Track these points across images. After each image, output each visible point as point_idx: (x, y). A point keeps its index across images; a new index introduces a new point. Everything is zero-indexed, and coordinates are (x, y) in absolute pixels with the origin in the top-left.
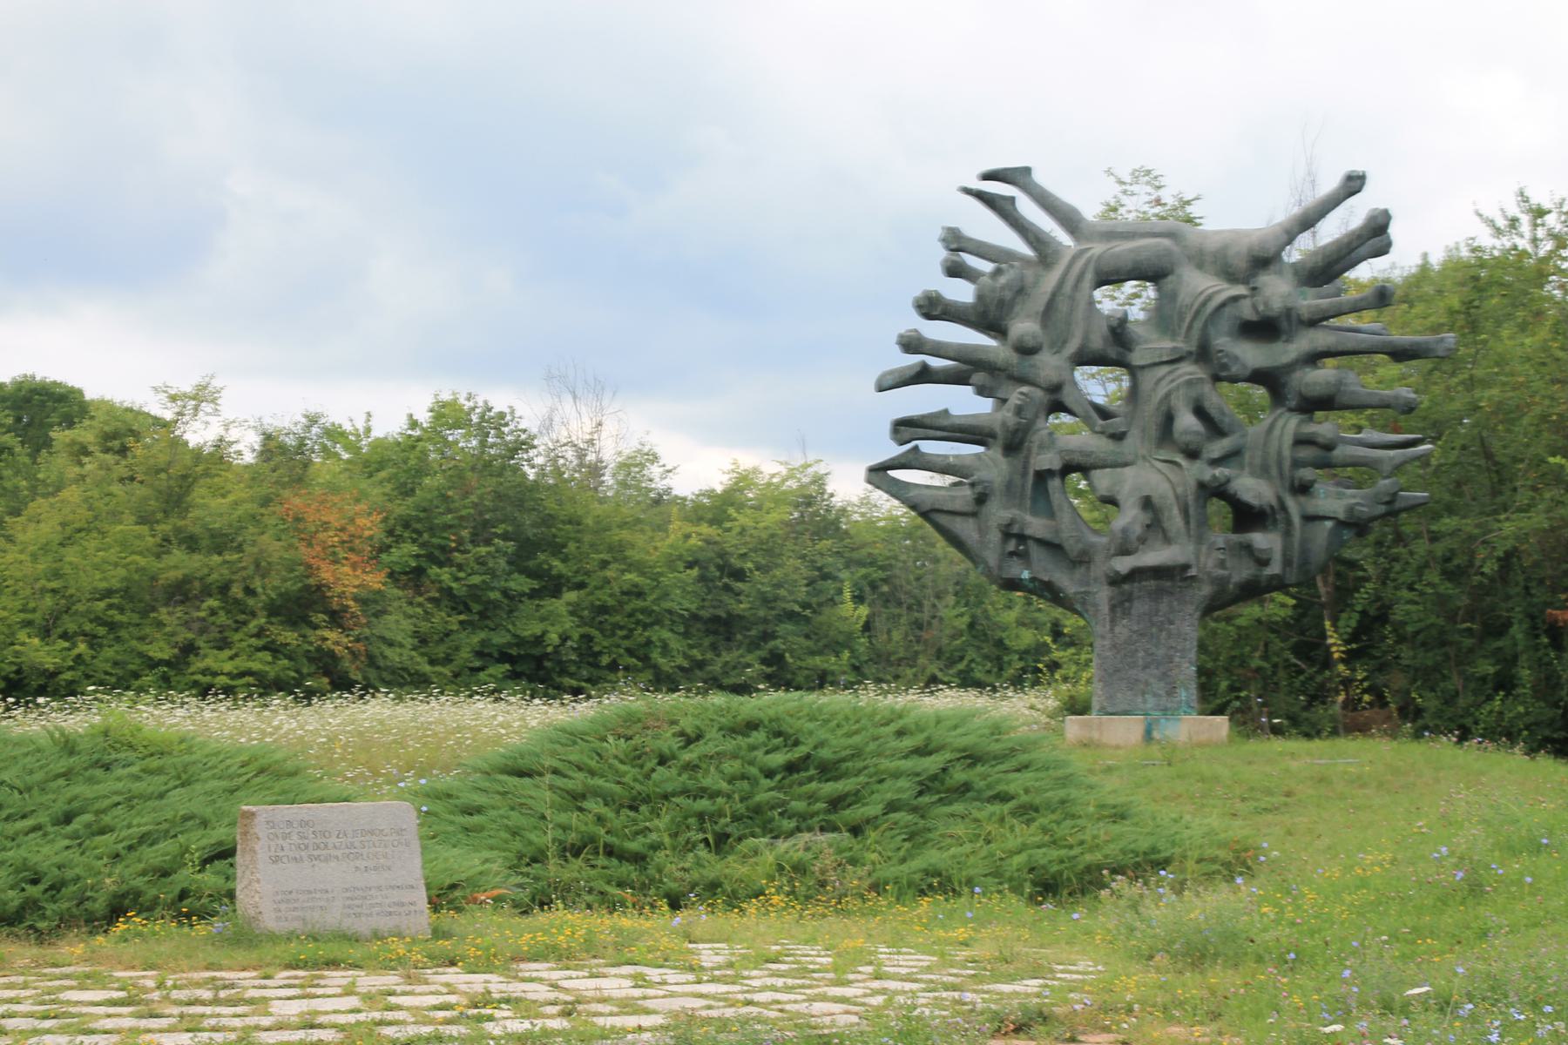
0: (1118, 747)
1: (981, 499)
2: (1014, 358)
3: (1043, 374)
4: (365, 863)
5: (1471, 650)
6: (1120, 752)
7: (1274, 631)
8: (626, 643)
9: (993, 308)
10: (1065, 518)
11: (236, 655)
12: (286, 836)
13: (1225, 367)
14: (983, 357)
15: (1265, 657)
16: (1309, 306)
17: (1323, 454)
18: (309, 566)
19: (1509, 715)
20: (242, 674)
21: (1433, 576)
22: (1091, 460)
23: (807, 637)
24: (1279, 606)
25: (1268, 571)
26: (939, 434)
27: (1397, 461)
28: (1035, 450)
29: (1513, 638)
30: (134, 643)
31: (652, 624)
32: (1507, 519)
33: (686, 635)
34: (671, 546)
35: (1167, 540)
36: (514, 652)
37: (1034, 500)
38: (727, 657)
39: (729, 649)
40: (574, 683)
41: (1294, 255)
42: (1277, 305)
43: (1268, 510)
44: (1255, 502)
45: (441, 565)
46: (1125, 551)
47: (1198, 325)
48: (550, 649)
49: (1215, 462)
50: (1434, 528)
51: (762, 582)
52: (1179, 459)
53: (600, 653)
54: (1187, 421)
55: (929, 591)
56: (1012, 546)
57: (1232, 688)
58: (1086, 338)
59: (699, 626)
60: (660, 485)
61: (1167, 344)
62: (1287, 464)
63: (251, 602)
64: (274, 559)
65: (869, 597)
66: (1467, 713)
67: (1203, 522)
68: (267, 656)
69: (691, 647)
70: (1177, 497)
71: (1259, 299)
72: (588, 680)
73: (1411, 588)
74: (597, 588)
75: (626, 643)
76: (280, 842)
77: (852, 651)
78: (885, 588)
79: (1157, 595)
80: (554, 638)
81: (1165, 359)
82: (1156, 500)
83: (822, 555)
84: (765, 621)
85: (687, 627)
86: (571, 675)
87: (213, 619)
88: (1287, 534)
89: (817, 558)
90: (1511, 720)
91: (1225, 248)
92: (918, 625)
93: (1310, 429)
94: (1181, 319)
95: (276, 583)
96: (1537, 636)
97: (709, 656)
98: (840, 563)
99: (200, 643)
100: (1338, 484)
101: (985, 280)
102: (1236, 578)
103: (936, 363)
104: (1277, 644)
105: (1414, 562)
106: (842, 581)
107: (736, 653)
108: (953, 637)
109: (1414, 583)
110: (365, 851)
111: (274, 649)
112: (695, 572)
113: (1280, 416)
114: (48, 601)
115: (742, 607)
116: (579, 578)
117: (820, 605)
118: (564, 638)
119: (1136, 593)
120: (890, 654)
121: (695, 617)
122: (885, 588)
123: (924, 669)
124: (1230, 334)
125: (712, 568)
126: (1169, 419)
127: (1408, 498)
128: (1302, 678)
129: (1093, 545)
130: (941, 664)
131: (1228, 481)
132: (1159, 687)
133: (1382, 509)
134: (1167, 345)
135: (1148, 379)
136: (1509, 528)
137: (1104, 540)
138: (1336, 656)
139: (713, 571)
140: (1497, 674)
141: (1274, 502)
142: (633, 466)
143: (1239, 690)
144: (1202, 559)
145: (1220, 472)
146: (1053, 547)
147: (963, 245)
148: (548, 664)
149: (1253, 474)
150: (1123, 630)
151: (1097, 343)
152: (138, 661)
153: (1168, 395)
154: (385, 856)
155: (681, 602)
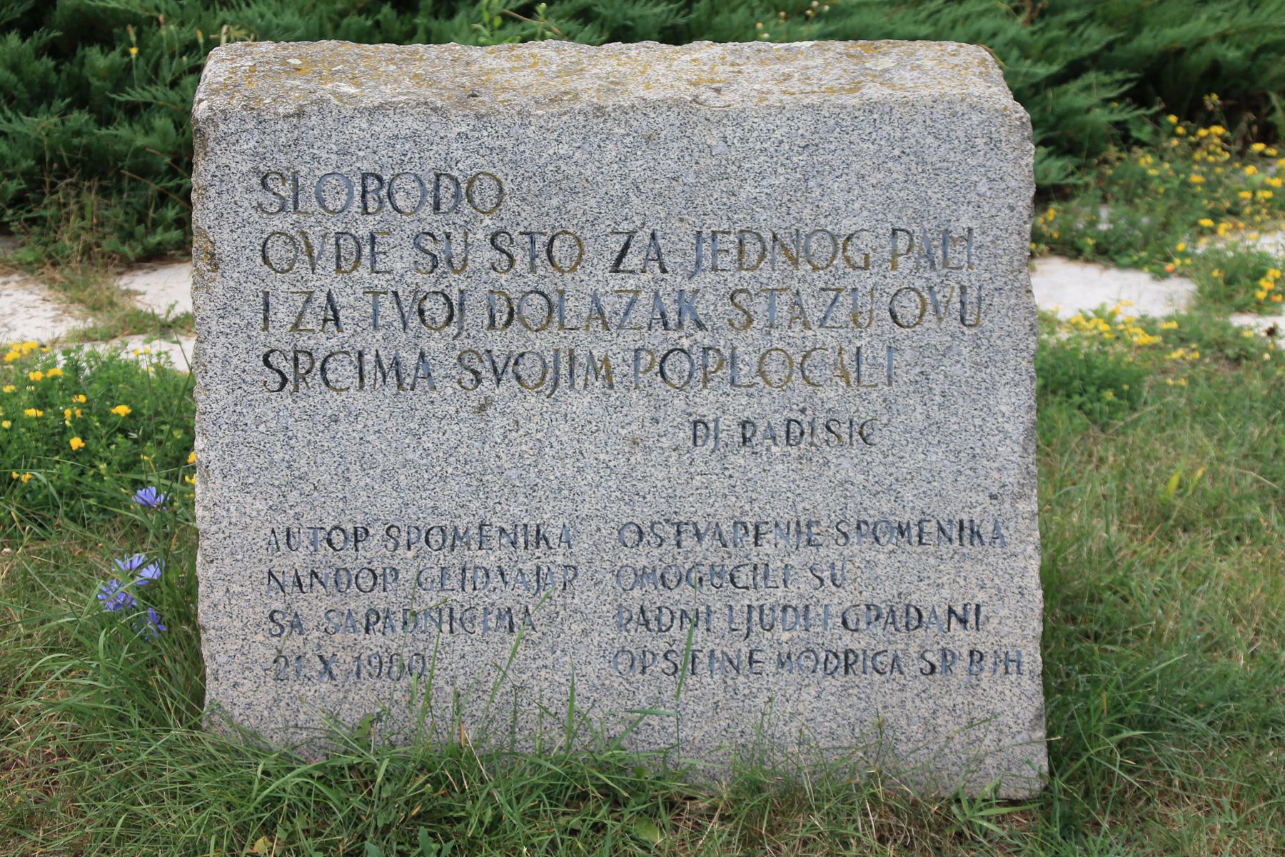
4: (740, 405)
12: (358, 252)
76: (325, 279)
110: (747, 345)
154: (851, 371)
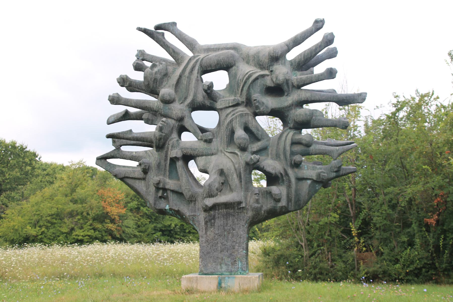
1: (145, 171)
2: (161, 105)
3: (174, 112)
5: (399, 232)
9: (151, 83)
11: (85, 231)
13: (257, 107)
17: (306, 147)
18: (104, 207)
19: (412, 255)
20: (86, 236)
21: (385, 207)
22: (196, 153)
25: (280, 205)
27: (340, 152)
28: (170, 148)
29: (413, 228)
30: (58, 228)
32: (410, 187)
35: (231, 190)
36: (164, 229)
37: (170, 172)
40: (179, 237)
42: (281, 78)
43: (279, 175)
44: (273, 172)
45: (144, 207)
46: (211, 195)
47: (246, 88)
48: (172, 228)
52: (237, 151)
53: (186, 229)
54: (240, 133)
57: (318, 246)
58: (195, 95)
61: (233, 98)
62: (288, 154)
63: (88, 217)
64: (94, 205)
66: (398, 254)
68: (92, 231)
70: (236, 170)
71: (274, 76)
73: (378, 211)
79: (227, 216)
80: (173, 225)
81: (231, 105)
82: (225, 171)
86: (179, 235)
87: (79, 221)
88: (289, 187)
90: (413, 257)
91: (258, 53)
93: (297, 137)
94: (238, 86)
95: (95, 212)
96: (422, 228)
99: (75, 228)
101: (148, 70)
102: (265, 208)
103: (132, 110)
105: (380, 202)
111: (95, 229)
114: (36, 217)
118: (176, 225)
119: (217, 216)
124: (261, 92)
126: (233, 132)
127: (346, 169)
131: (258, 161)
132: (228, 261)
133: (334, 174)
136: (410, 190)
138: (354, 234)
140: (408, 241)
143: (320, 246)
144: (248, 199)
146: (179, 194)
148: (172, 232)
151: (201, 97)
152: (59, 232)
153: (231, 121)
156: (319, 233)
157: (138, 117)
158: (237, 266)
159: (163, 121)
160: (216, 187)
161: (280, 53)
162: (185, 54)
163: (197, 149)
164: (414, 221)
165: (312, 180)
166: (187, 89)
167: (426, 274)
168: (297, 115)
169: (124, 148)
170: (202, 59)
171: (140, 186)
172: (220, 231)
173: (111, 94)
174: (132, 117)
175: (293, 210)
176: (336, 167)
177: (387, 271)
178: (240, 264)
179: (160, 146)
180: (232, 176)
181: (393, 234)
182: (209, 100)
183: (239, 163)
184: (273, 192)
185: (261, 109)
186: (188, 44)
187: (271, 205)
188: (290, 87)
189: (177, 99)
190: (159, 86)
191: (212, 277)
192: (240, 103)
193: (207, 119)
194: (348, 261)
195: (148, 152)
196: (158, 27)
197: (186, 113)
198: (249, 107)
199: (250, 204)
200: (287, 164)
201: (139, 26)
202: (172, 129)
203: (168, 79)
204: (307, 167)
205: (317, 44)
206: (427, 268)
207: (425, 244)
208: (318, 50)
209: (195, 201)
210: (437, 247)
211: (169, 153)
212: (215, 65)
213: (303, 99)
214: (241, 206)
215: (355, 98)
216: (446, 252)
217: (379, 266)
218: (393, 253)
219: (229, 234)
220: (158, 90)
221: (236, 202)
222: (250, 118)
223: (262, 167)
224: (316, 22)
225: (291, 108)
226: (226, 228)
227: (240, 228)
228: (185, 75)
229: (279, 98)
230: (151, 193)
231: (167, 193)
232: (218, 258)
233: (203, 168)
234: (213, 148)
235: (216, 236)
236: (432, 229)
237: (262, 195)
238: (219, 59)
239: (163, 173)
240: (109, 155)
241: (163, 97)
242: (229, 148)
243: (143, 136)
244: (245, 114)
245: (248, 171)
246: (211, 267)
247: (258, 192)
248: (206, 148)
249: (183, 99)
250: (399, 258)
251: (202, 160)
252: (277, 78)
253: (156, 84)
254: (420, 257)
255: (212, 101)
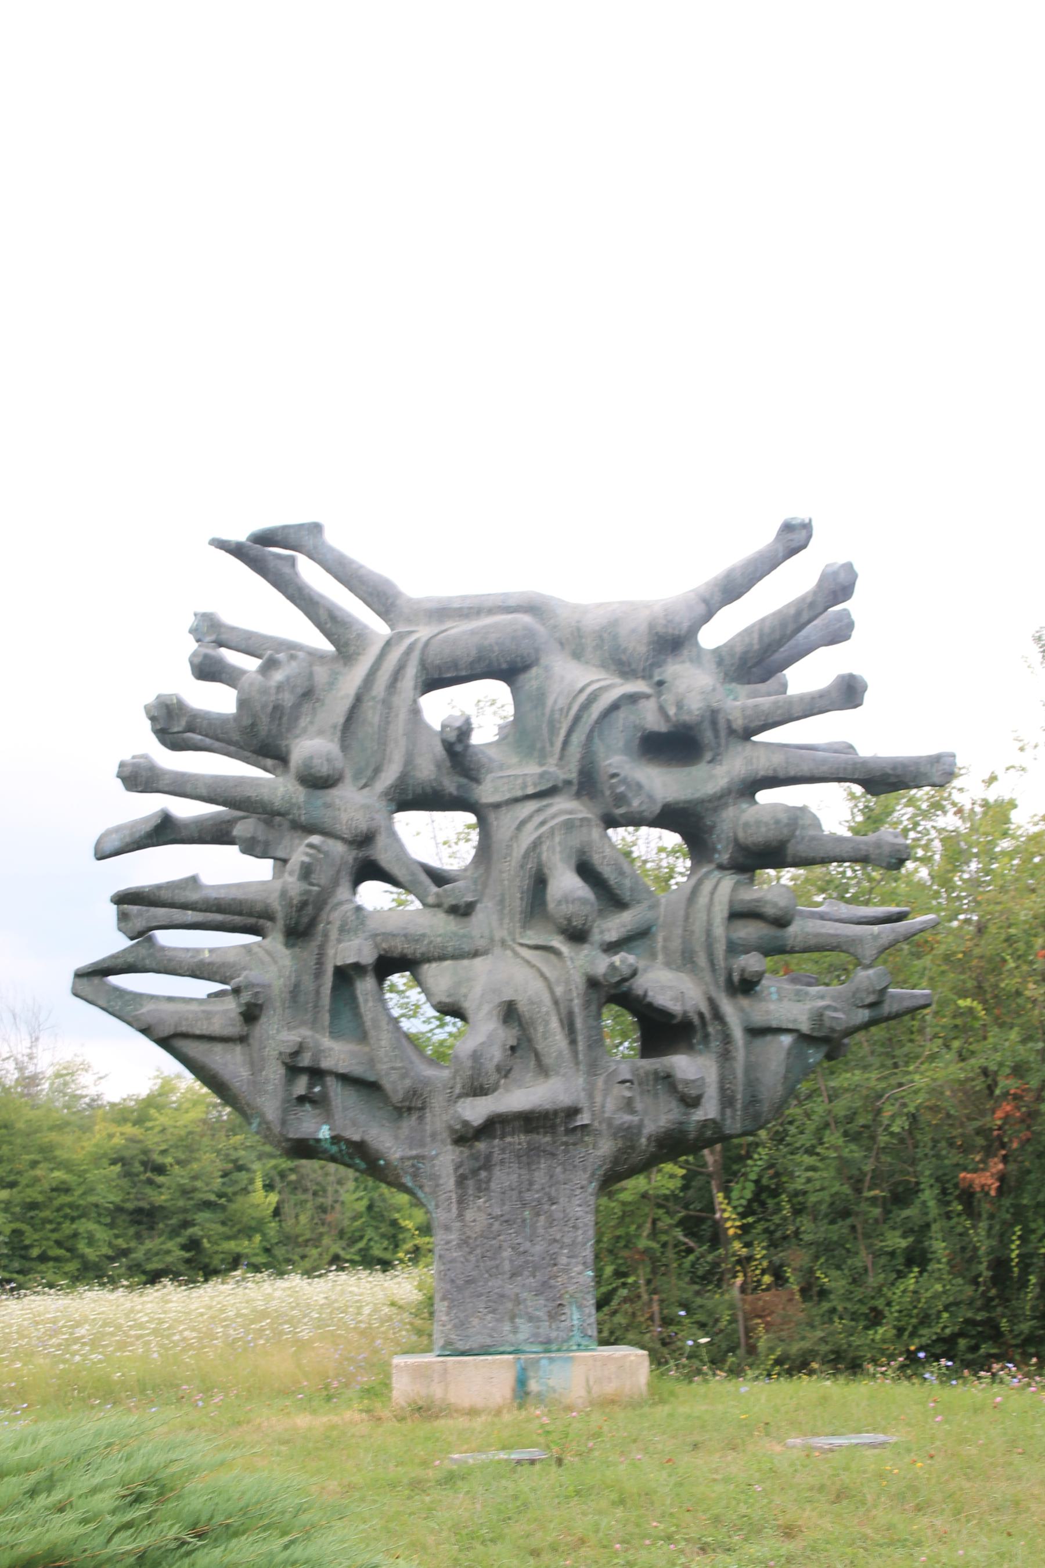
0: (472, 1412)
1: (251, 1014)
3: (344, 817)
6: (478, 1423)
7: (660, 1206)
8: (55, 1236)
9: (265, 719)
10: (383, 1040)
13: (620, 799)
14: (252, 793)
15: (654, 1234)
16: (743, 709)
17: (771, 929)
21: (834, 1137)
22: (420, 949)
23: (223, 1223)
24: (667, 1177)
25: (699, 1115)
26: (190, 916)
27: (884, 941)
28: (334, 935)
31: (80, 1217)
33: (111, 1226)
34: (96, 1145)
35: (543, 1070)
37: (334, 1014)
38: (149, 1244)
39: (152, 1237)
41: (713, 636)
42: (695, 705)
43: (696, 1020)
46: (478, 1090)
47: (578, 738)
49: (611, 948)
50: (832, 1084)
51: (179, 1175)
52: (557, 942)
54: (566, 884)
55: (331, 1178)
56: (301, 1086)
58: (409, 761)
59: (124, 1217)
60: (92, 1091)
61: (533, 769)
62: (720, 948)
65: (279, 1185)
67: (596, 1041)
69: (117, 1236)
70: (556, 1003)
71: (669, 699)
72: (19, 1272)
73: (810, 1151)
74: (27, 1186)
75: (55, 1236)
77: (264, 1235)
78: (293, 1177)
79: (529, 1157)
81: (530, 791)
82: (523, 1007)
83: (236, 1149)
84: (185, 1211)
85: (113, 1219)
88: (725, 1056)
89: (231, 1152)
91: (614, 623)
92: (323, 1209)
93: (751, 894)
94: (553, 729)
96: (948, 1203)
97: (133, 1244)
98: (253, 1156)
100: (794, 981)
103: (187, 810)
104: (666, 1221)
106: (255, 1172)
107: (158, 1241)
108: (354, 1219)
109: (813, 1147)
112: (117, 1168)
113: (707, 875)
115: (161, 1198)
116: (12, 1178)
117: (235, 1194)
119: (497, 1157)
120: (297, 1236)
121: (119, 1209)
122: (293, 1177)
123: (328, 1249)
124: (627, 750)
125: (137, 1164)
126: (540, 882)
127: (901, 998)
128: (692, 1257)
129: (427, 1082)
130: (343, 1243)
131: (634, 973)
132: (538, 1306)
133: (864, 1015)
134: (529, 772)
135: (504, 824)
137: (446, 1074)
138: (731, 1232)
139: (138, 1168)
141: (704, 1008)
142: (65, 1075)
143: (625, 1275)
144: (598, 1099)
145: (622, 960)
146: (366, 1087)
147: (224, 637)
149: (668, 964)
150: (478, 1215)
151: (428, 768)
153: (536, 845)
155: (108, 1196)
156: (619, 1232)
157: (214, 834)
158: (567, 1323)
159: (311, 846)
160: (496, 1060)
161: (686, 625)
162: (366, 627)
163: (424, 935)
164: (926, 1180)
165: (795, 1035)
166: (383, 740)
167: (970, 1356)
168: (746, 825)
169: (165, 938)
170: (427, 644)
171: (230, 1062)
172: (506, 1208)
173: (127, 757)
174: (184, 834)
175: (739, 1131)
176: (874, 992)
177: (845, 1351)
178: (576, 1316)
179: (301, 928)
180: (547, 1023)
181: (859, 1228)
182: (452, 779)
183: (567, 982)
184: (680, 1074)
185: (635, 803)
186: (371, 594)
187: (671, 1117)
188: (723, 733)
189: (348, 775)
190: (289, 730)
191: (494, 1361)
192: (560, 785)
193: (435, 838)
194: (717, 1321)
195: (256, 949)
196: (265, 539)
197: (380, 818)
198: (585, 798)
199: (606, 1115)
200: (716, 982)
201: (211, 537)
202: (338, 872)
203: (314, 709)
204: (778, 992)
205: (803, 599)
206: (972, 1337)
207: (964, 1258)
208: (805, 617)
209: (422, 1108)
210: (1000, 1265)
211: (331, 952)
212: (472, 663)
213: (762, 773)
214: (579, 1123)
215: (922, 769)
216: (1033, 1279)
217: (820, 1334)
218: (859, 1293)
219: (538, 1215)
220: (284, 743)
221: (563, 1110)
222: (595, 833)
223: (640, 992)
224: (788, 528)
225: (723, 801)
226: (527, 1196)
227: (571, 1197)
228: (374, 693)
229: (687, 769)
230: (270, 1088)
231: (324, 1086)
232: (502, 1296)
233: (447, 1000)
234: (476, 933)
235: (496, 1226)
236: (986, 1207)
237: (640, 1084)
238: (486, 643)
239: (309, 1016)
240: (120, 961)
241: (307, 764)
242: (529, 933)
243: (239, 895)
244: (582, 820)
245: (594, 1007)
246: (479, 1331)
247: (628, 1077)
248: (455, 934)
249: (369, 773)
250: (881, 1307)
251: (441, 976)
252: (679, 705)
253: (279, 725)
254: (951, 1299)
255: (464, 781)
